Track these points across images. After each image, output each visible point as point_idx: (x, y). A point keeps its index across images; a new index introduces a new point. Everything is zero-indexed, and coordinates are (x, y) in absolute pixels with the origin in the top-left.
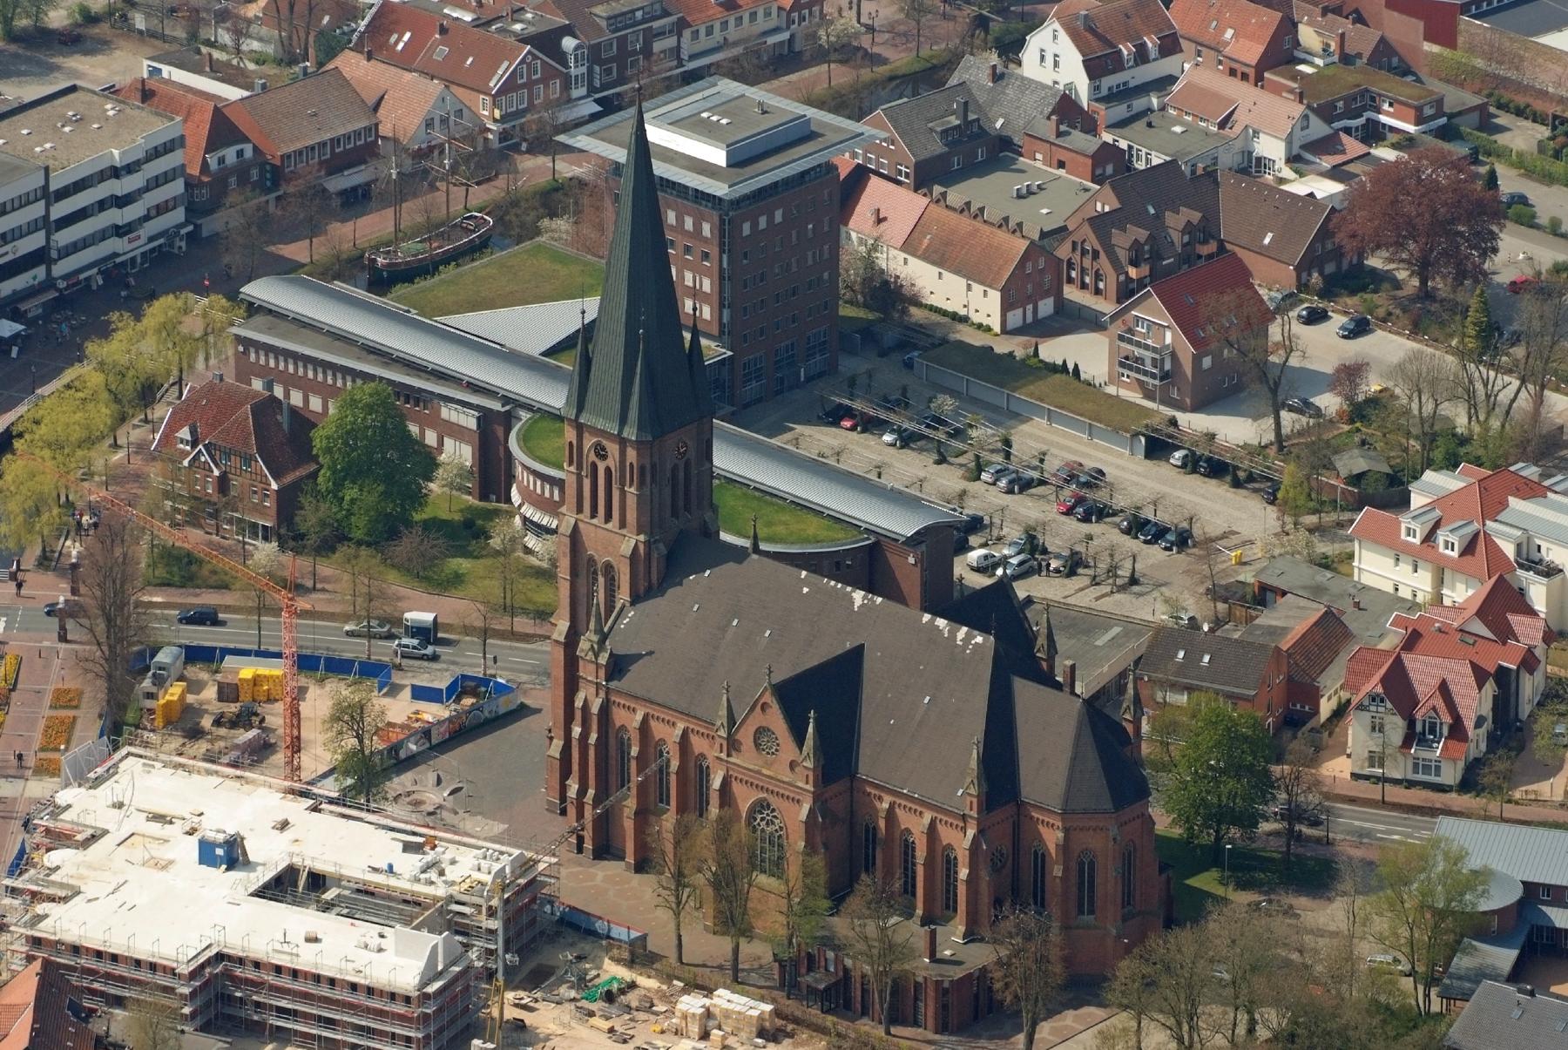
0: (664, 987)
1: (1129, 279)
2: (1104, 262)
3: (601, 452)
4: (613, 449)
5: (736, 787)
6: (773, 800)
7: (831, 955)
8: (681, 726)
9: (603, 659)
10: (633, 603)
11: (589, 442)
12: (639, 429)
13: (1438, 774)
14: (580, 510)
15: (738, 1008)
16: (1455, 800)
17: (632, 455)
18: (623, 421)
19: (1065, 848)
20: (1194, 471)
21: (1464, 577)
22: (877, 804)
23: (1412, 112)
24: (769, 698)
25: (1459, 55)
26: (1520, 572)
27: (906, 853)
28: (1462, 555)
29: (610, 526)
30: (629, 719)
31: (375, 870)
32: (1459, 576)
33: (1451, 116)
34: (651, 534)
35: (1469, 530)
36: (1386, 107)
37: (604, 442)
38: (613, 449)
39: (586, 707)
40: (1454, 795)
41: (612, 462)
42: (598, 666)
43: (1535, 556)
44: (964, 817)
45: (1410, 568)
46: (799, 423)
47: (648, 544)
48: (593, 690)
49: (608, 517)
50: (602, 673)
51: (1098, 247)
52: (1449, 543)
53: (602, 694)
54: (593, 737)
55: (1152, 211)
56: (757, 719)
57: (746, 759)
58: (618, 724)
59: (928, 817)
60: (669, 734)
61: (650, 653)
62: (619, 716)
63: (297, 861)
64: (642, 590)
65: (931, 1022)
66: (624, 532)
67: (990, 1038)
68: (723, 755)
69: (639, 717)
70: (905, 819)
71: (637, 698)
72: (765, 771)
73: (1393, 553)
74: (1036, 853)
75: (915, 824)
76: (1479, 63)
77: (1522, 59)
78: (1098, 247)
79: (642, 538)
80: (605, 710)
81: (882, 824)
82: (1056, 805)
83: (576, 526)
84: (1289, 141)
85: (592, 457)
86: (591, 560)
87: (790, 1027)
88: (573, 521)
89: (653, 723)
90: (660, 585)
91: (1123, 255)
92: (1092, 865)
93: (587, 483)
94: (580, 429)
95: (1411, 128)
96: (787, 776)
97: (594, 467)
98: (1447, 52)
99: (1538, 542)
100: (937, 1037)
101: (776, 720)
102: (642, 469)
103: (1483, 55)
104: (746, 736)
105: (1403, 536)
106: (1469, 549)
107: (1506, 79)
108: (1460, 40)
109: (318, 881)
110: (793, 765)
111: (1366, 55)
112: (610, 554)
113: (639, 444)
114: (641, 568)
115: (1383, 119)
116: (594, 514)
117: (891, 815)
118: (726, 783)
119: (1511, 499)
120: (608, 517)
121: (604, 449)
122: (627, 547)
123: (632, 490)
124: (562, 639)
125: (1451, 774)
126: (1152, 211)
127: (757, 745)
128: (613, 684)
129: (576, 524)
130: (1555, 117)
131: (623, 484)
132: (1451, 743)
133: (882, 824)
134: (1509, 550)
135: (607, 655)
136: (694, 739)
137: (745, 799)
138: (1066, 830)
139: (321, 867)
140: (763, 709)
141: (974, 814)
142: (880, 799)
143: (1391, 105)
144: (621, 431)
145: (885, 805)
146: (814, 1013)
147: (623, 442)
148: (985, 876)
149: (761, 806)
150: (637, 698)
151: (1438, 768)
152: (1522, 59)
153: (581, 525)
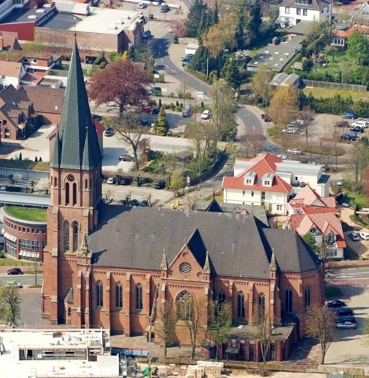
0: (168, 367)
1: (19, 130)
2: (9, 125)
3: (71, 178)
4: (77, 176)
5: (170, 289)
6: (188, 290)
7: (234, 341)
8: (128, 274)
9: (90, 256)
10: (89, 234)
11: (64, 176)
12: (90, 165)
13: (336, 255)
14: (60, 203)
15: (209, 365)
16: (343, 263)
17: (86, 176)
18: (81, 165)
19: (302, 286)
20: (119, 184)
21: (276, 193)
22: (227, 285)
23: (46, 62)
24: (187, 250)
25: (36, 43)
26: (293, 188)
27: (239, 301)
28: (273, 185)
29: (75, 206)
30: (103, 277)
31: (53, 344)
32: (273, 193)
33: (55, 62)
34: (93, 207)
35: (272, 175)
36: (32, 62)
37: (73, 174)
38: (77, 176)
39: (82, 277)
40: (343, 262)
41: (77, 181)
42: (87, 259)
43: (296, 182)
44: (269, 280)
45: (251, 195)
46: (42, 177)
47: (93, 210)
48: (85, 269)
49: (75, 202)
50: (89, 261)
51: (6, 119)
52: (267, 179)
53: (89, 270)
54: (87, 287)
55: (14, 104)
56: (181, 260)
57: (176, 275)
58: (96, 280)
59: (251, 284)
60: (123, 279)
61: (105, 250)
62: (97, 277)
63: (22, 347)
64: (91, 230)
65: (278, 357)
66: (82, 207)
67: (301, 359)
68: (165, 278)
69: (108, 274)
70: (239, 287)
71: (106, 267)
72: (185, 280)
73: (242, 191)
74: (287, 291)
75: (246, 289)
76: (46, 44)
77: (66, 39)
78: (6, 119)
79: (92, 208)
80: (91, 276)
81: (231, 291)
82: (297, 269)
83: (59, 212)
84: (19, 77)
85: (67, 181)
86: (67, 222)
87: (228, 370)
88: (57, 208)
89: (114, 276)
90: (98, 223)
91: (16, 121)
92: (309, 290)
93: (63, 193)
94: (60, 170)
95: (47, 68)
96: (196, 279)
97: (67, 185)
98: (30, 42)
99: (296, 176)
100: (282, 362)
101: (191, 258)
102: (91, 181)
103: (47, 40)
104: (176, 269)
105: (245, 183)
106: (275, 182)
107: (60, 48)
108: (36, 37)
109: (30, 354)
110: (198, 274)
111: (12, 45)
112: (76, 218)
113: (90, 172)
114: (92, 220)
115: (32, 67)
116: (67, 202)
117: (234, 288)
118: (166, 288)
119: (276, 164)
120: (75, 202)
121: (72, 176)
122: (86, 213)
123: (87, 190)
124: (56, 255)
125: (340, 254)
126: (14, 104)
127: (181, 270)
128: (95, 264)
129: (59, 209)
130: (87, 57)
131: (81, 188)
132: (339, 242)
133: (231, 291)
134: (288, 181)
135: (91, 254)
136: (134, 278)
137: (175, 293)
138: (302, 279)
139: (31, 347)
140: (184, 255)
141: (274, 278)
142: (228, 282)
143: (35, 61)
144: (81, 167)
145: (231, 284)
146: (237, 364)
147: (81, 172)
148: (279, 301)
149: (182, 294)
150: (106, 267)
151: (336, 252)
152: (66, 39)
153: (61, 209)
